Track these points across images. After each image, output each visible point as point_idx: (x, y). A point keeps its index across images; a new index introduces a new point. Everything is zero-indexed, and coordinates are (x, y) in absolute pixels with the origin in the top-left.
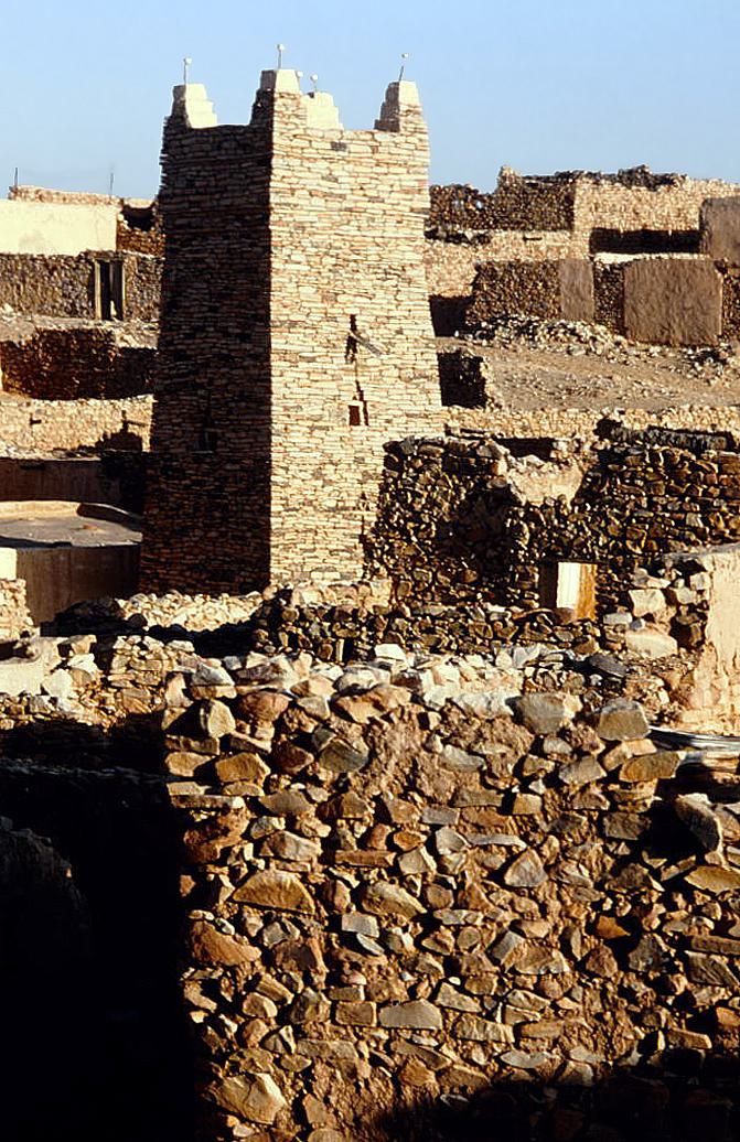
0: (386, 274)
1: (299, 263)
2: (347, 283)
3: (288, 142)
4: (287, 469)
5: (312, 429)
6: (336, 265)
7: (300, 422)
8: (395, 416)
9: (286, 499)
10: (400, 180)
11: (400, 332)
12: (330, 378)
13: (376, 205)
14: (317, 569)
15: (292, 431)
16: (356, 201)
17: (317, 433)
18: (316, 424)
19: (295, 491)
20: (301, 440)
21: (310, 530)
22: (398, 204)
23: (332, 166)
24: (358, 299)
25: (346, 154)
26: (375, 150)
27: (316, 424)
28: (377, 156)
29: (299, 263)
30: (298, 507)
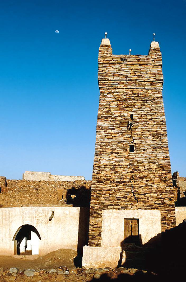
0: (147, 101)
1: (111, 98)
2: (130, 104)
3: (104, 59)
4: (99, 167)
5: (112, 153)
6: (126, 98)
7: (106, 151)
8: (147, 148)
9: (99, 178)
10: (150, 70)
11: (151, 119)
12: (120, 135)
13: (140, 78)
14: (111, 205)
15: (103, 154)
16: (132, 77)
17: (114, 155)
18: (113, 151)
19: (103, 175)
20: (106, 156)
21: (109, 190)
22: (149, 78)
23: (122, 66)
24: (134, 109)
25: (127, 62)
26: (139, 61)
27: (113, 151)
28: (140, 63)
29: (111, 98)
30: (103, 181)
